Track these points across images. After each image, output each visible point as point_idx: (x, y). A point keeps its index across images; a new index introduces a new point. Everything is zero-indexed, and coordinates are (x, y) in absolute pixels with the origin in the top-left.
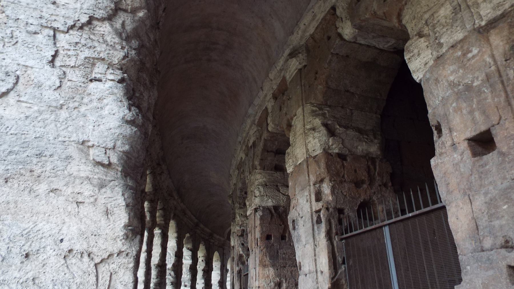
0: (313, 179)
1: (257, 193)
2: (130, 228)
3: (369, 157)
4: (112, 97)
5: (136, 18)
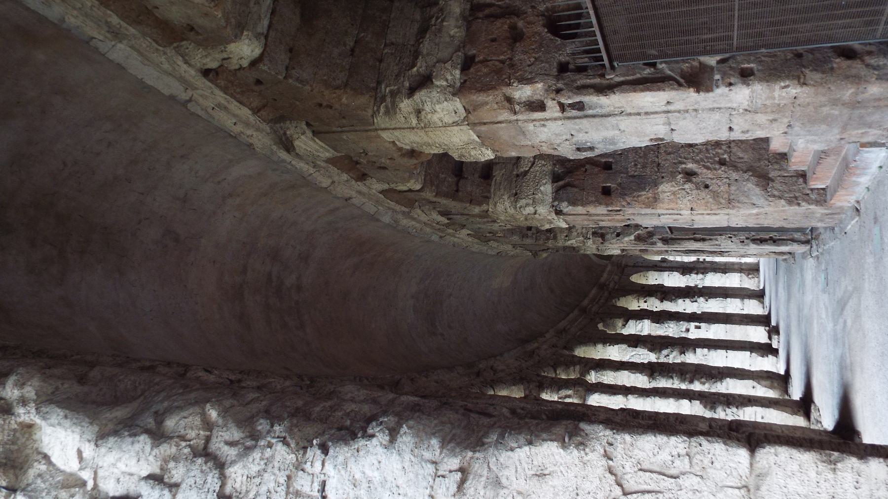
0: (505, 115)
1: (530, 210)
2: (567, 440)
3: (470, 15)
4: (352, 464)
5: (220, 421)
